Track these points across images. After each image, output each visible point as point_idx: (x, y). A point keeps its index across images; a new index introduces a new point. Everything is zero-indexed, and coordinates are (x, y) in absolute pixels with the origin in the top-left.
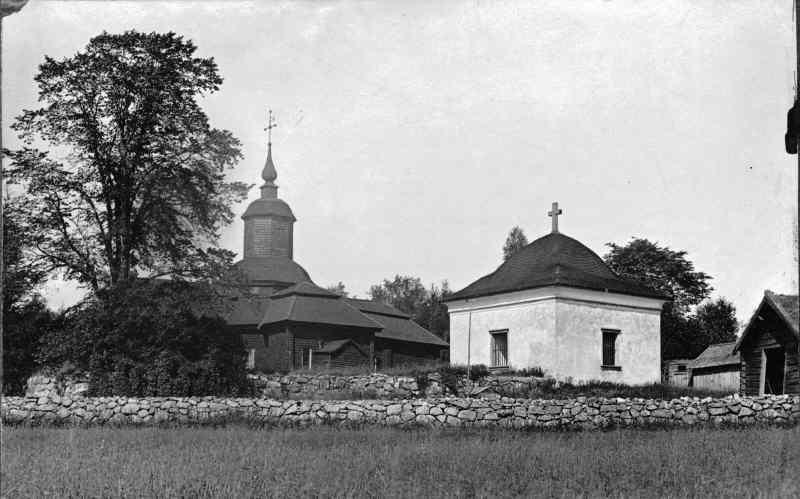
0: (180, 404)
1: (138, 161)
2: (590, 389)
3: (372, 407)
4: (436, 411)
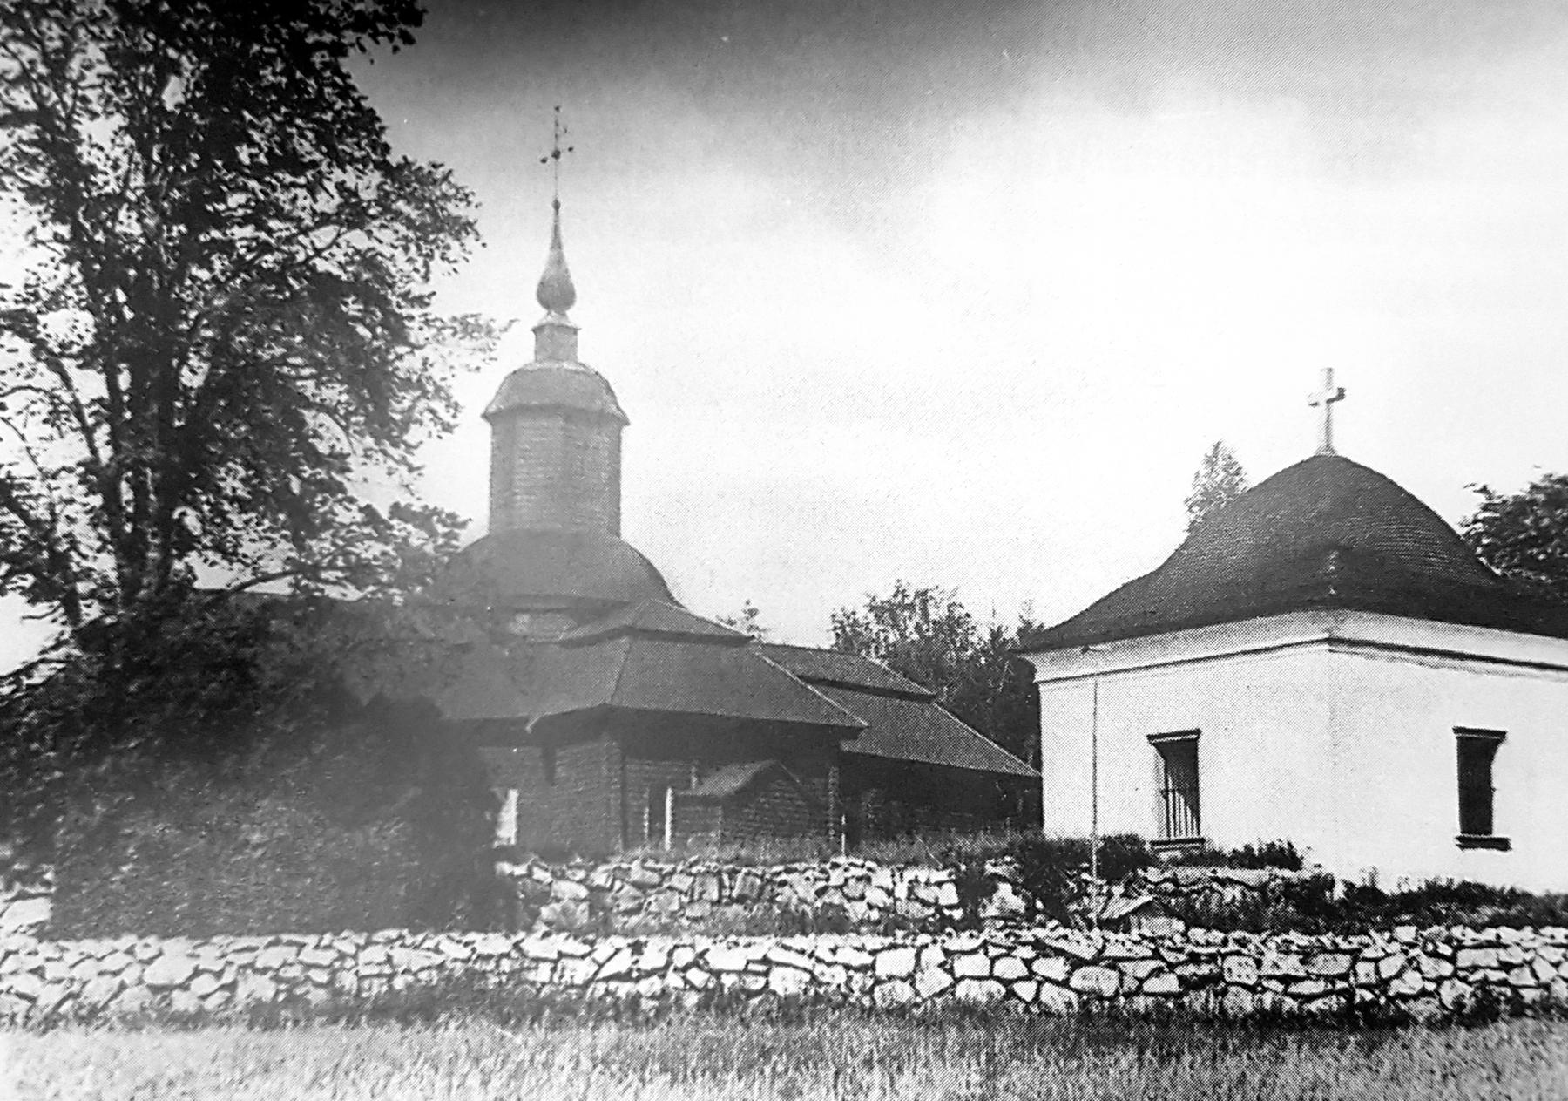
0: (308, 955)
1: (193, 253)
2: (1434, 904)
3: (837, 957)
4: (1010, 968)
